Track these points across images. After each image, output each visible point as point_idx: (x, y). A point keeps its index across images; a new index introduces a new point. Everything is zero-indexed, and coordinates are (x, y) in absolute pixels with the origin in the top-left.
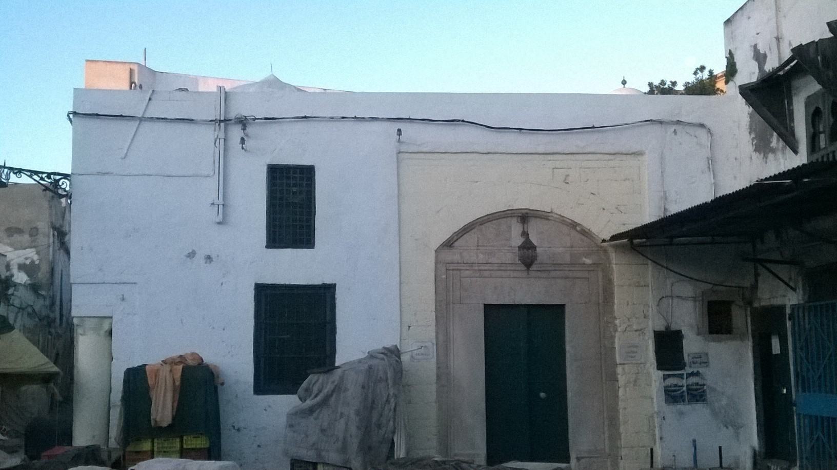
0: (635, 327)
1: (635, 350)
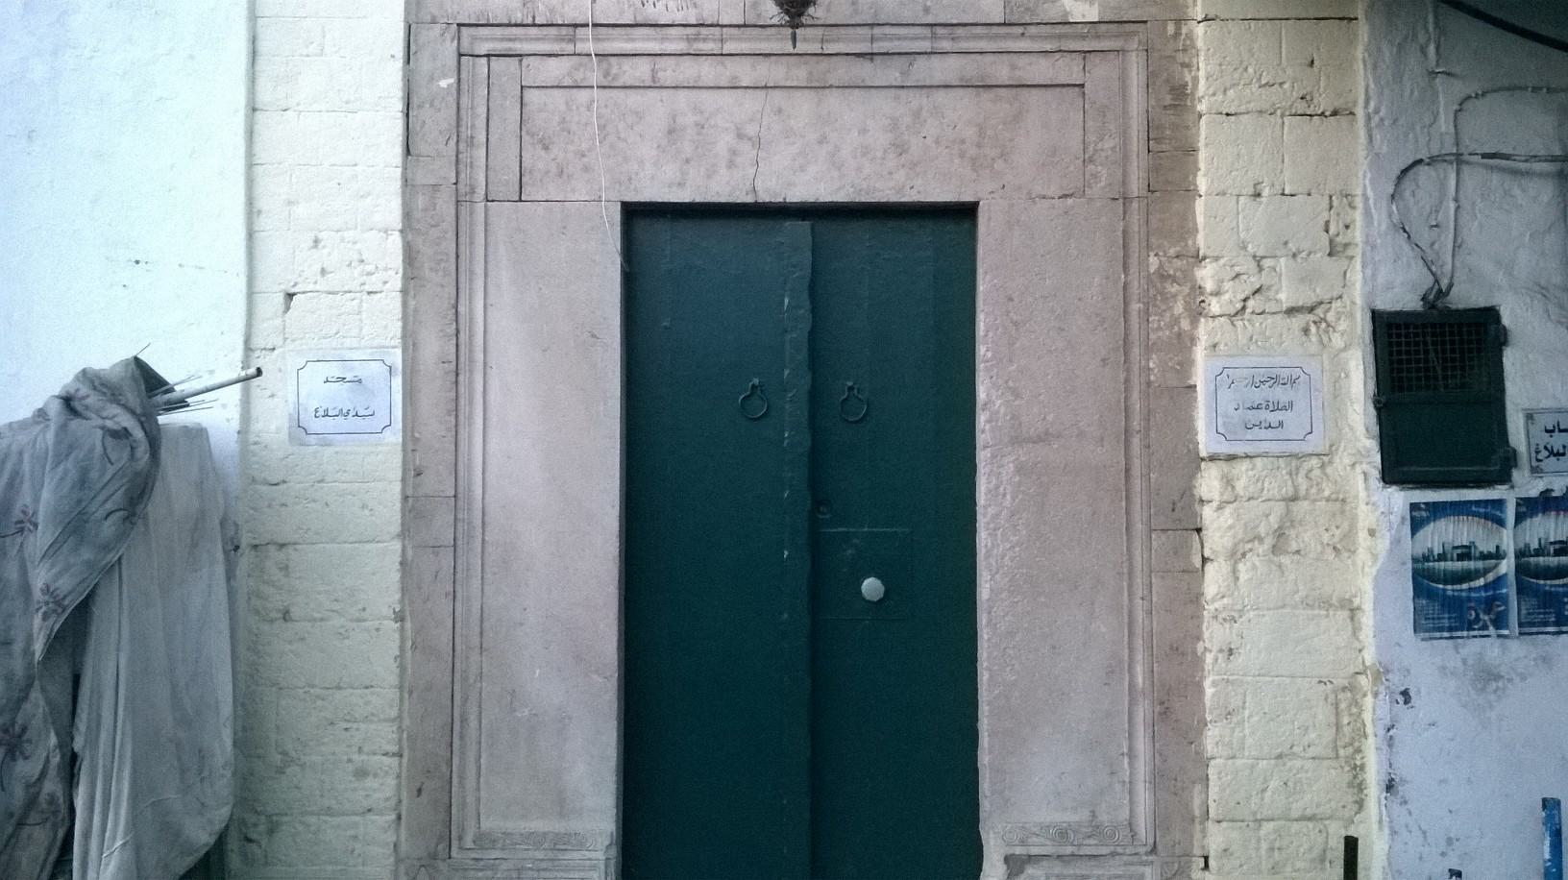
0: (1285, 297)
1: (1280, 394)
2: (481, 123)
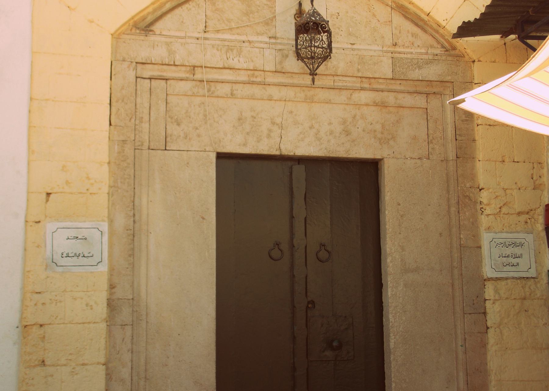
1: (517, 251)
2: (146, 111)
